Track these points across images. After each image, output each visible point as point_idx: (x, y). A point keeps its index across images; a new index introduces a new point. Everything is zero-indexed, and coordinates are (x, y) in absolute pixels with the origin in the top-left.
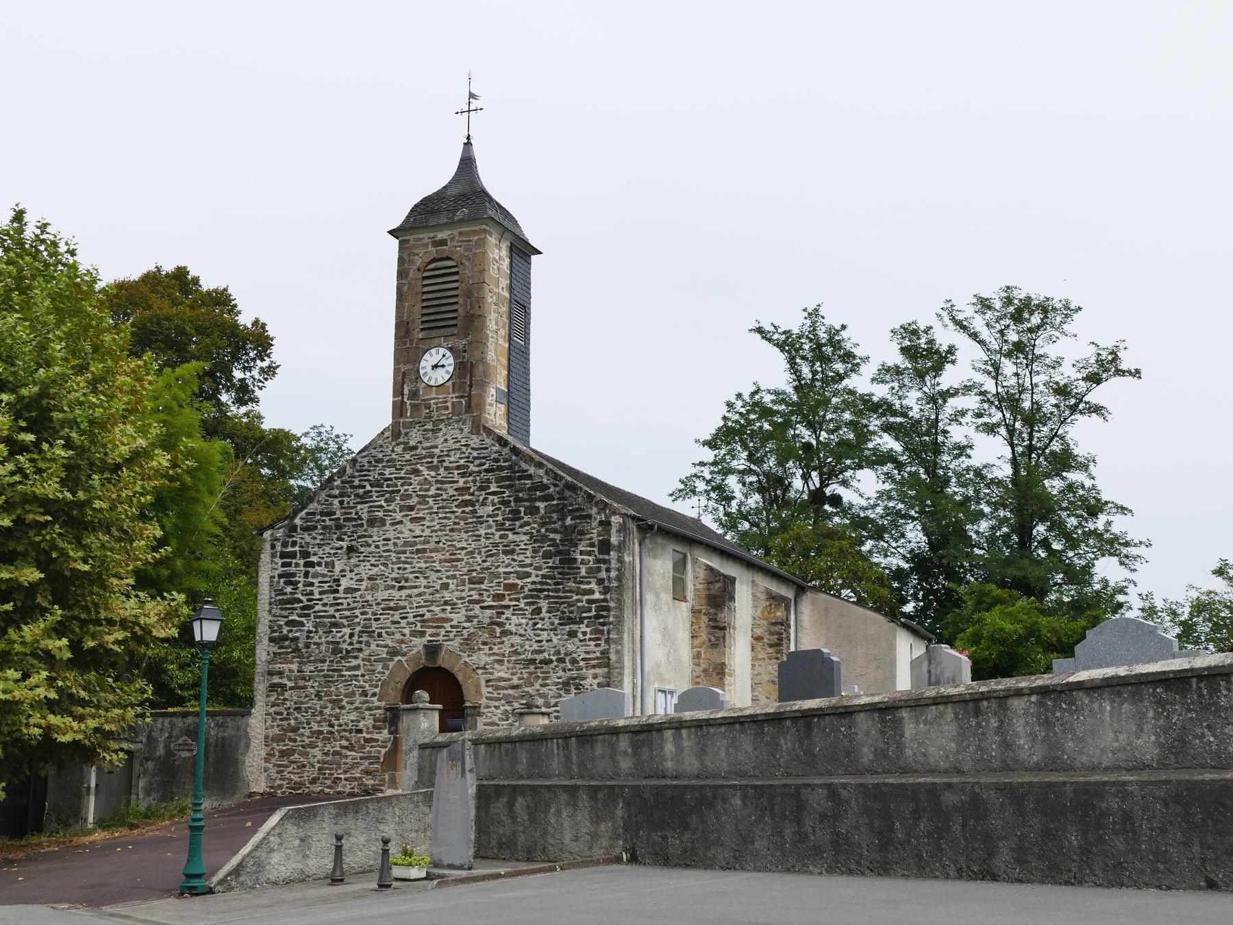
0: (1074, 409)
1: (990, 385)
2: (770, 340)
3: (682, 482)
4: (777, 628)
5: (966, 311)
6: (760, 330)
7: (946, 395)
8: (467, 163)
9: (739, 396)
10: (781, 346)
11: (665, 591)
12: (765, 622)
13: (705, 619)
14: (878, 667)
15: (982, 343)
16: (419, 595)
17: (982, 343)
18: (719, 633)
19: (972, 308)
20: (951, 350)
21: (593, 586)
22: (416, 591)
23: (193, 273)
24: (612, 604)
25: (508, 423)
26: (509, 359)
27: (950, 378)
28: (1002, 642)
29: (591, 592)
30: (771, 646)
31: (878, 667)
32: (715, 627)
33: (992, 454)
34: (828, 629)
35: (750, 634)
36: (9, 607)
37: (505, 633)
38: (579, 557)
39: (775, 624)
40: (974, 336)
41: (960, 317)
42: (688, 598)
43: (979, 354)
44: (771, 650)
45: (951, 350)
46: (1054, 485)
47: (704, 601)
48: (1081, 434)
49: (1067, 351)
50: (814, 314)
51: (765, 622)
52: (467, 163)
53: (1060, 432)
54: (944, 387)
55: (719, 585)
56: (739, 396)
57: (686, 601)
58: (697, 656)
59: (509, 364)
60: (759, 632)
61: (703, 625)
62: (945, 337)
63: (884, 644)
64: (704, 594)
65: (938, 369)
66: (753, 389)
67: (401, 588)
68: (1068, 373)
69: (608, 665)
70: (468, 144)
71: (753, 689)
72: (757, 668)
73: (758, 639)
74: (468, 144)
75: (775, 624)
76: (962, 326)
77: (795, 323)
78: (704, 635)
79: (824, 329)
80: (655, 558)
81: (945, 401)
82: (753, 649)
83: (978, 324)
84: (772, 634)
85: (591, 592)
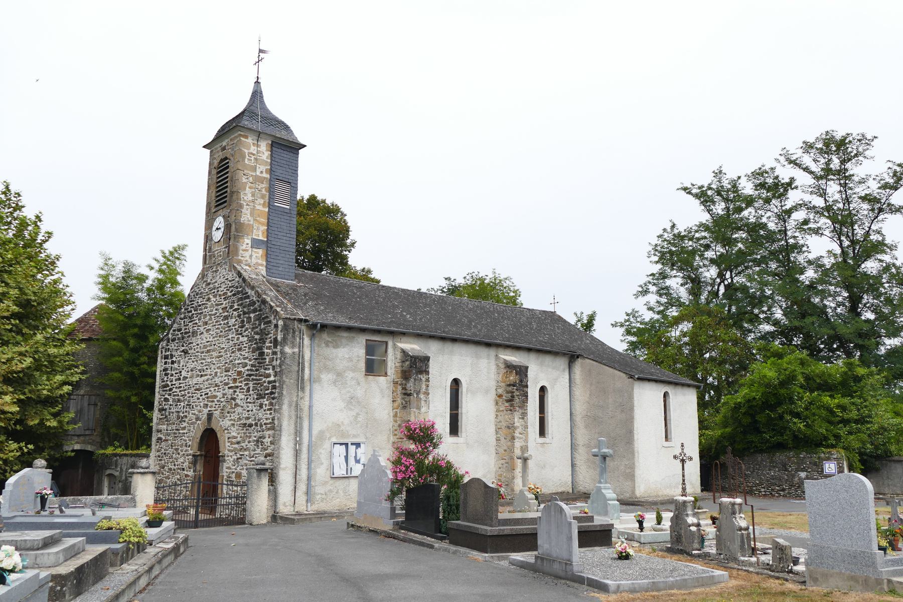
0: (881, 210)
1: (819, 202)
2: (689, 193)
3: (641, 286)
4: (510, 388)
5: (797, 154)
6: (685, 189)
7: (789, 212)
8: (257, 95)
9: (665, 230)
10: (696, 196)
11: (354, 369)
12: (503, 384)
13: (400, 388)
14: (622, 411)
15: (811, 173)
16: (207, 380)
17: (811, 173)
18: (407, 398)
19: (801, 150)
20: (792, 180)
21: (271, 371)
22: (206, 378)
23: (320, 198)
24: (277, 384)
25: (267, 261)
26: (268, 219)
27: (793, 198)
28: (768, 385)
29: (269, 376)
30: (507, 401)
31: (622, 411)
32: (405, 394)
33: (821, 247)
34: (591, 384)
35: (494, 392)
36: (891, 342)
37: (237, 405)
38: (266, 351)
39: (509, 385)
40: (806, 169)
41: (794, 158)
42: (389, 374)
43: (808, 180)
44: (507, 404)
45: (792, 180)
46: (871, 266)
47: (400, 375)
48: (891, 228)
49: (870, 170)
50: (719, 174)
51: (503, 384)
52: (257, 95)
53: (874, 227)
54: (788, 207)
55: (408, 363)
56: (665, 230)
57: (386, 375)
58: (395, 416)
59: (268, 222)
60: (500, 391)
61: (399, 392)
62: (785, 173)
63: (626, 394)
64: (399, 370)
65: (782, 196)
66: (671, 224)
67: (202, 376)
68: (873, 187)
69: (273, 428)
70: (257, 83)
71: (497, 433)
72: (499, 417)
73: (500, 396)
74: (257, 83)
75: (509, 385)
76: (794, 163)
77: (705, 179)
78: (399, 401)
79: (727, 181)
80: (336, 346)
81: (789, 217)
82: (497, 403)
83: (807, 160)
84: (508, 392)
85: (269, 376)
